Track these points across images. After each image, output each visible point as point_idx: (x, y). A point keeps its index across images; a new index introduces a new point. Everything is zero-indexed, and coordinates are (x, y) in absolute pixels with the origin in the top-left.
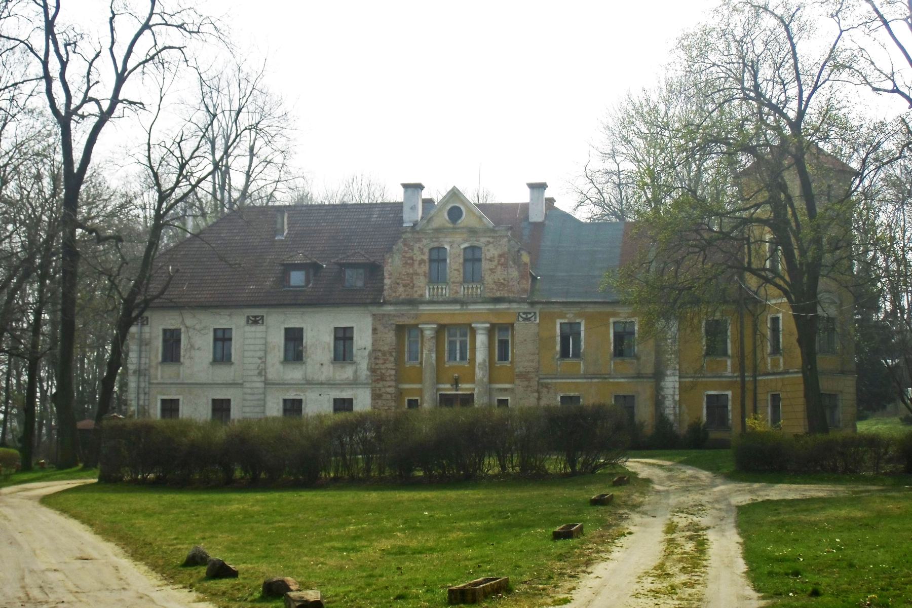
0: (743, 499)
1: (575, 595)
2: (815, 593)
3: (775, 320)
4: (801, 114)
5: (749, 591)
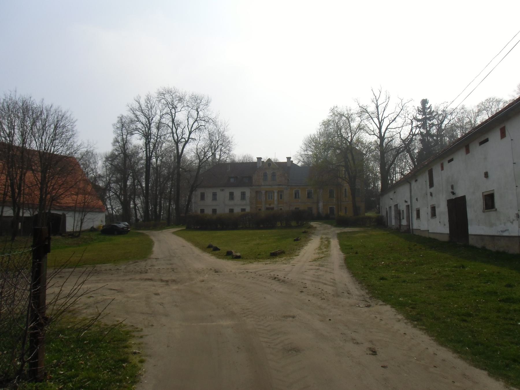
0: (338, 232)
1: (300, 254)
2: (357, 253)
3: (346, 189)
4: (352, 140)
5: (341, 253)
